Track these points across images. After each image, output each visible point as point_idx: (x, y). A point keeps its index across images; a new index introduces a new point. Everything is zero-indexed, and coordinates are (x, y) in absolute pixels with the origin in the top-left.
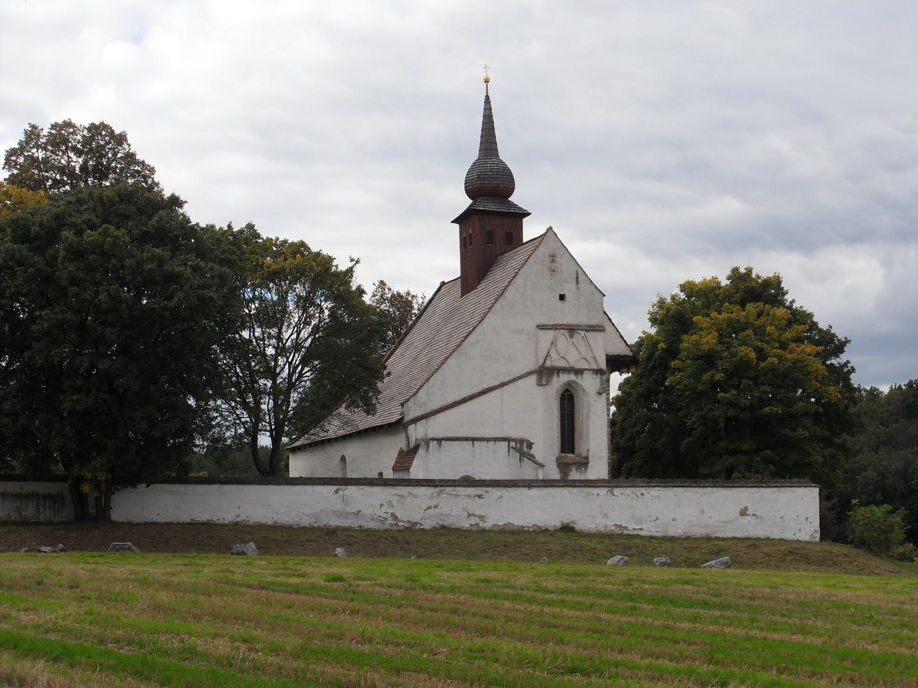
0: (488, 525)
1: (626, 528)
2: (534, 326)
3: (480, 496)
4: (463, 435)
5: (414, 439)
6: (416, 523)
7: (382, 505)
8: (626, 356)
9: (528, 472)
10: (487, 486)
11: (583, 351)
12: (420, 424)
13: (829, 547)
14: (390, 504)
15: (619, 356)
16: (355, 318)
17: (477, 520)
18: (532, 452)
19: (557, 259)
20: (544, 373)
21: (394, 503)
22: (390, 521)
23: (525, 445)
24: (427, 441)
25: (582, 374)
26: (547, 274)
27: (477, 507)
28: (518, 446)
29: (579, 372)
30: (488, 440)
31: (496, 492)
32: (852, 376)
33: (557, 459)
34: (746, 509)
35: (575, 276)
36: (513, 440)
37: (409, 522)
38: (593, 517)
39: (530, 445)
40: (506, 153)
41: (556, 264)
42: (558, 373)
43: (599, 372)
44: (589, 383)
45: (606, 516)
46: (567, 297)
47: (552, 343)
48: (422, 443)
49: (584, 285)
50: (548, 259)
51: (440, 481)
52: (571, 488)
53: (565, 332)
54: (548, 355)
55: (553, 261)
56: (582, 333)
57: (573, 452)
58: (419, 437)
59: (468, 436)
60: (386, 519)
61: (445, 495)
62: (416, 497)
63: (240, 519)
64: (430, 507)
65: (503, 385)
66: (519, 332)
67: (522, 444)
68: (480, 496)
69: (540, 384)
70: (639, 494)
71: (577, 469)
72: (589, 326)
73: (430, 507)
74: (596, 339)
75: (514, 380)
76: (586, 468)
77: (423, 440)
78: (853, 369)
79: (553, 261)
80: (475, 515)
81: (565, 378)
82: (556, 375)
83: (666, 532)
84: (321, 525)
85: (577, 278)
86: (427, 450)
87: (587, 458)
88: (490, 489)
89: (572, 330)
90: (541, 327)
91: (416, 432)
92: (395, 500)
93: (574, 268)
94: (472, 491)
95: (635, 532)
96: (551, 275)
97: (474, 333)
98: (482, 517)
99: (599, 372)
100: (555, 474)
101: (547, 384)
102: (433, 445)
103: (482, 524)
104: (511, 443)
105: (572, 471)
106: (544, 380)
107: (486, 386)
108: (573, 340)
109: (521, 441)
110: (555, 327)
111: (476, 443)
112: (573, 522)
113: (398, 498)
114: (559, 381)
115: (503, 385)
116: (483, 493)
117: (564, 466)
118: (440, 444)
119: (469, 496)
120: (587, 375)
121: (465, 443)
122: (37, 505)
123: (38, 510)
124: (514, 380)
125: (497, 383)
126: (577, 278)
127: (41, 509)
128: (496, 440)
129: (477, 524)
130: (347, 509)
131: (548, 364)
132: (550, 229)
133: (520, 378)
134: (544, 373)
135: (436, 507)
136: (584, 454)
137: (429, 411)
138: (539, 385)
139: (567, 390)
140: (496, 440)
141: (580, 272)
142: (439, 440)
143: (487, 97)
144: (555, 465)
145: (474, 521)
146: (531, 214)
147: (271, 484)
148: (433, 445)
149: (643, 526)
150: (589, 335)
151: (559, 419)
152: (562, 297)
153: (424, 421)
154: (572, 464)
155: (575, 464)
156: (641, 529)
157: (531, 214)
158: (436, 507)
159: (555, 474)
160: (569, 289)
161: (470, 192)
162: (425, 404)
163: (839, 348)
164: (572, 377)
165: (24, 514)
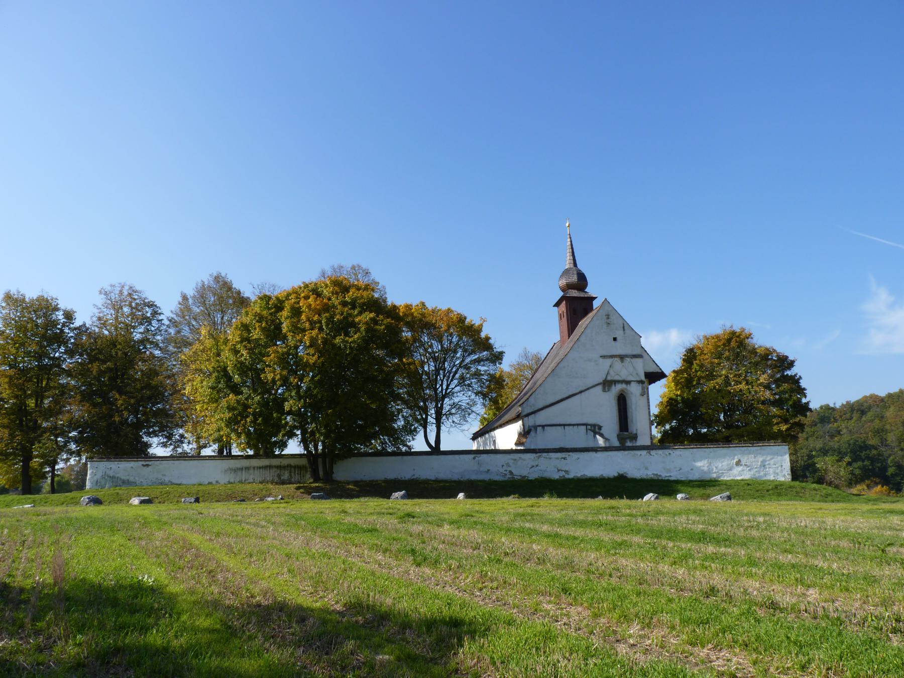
0: (571, 476)
1: (660, 476)
3: (564, 458)
4: (558, 423)
6: (525, 476)
7: (503, 466)
10: (569, 452)
12: (530, 417)
13: (797, 483)
14: (508, 465)
17: (564, 473)
18: (601, 432)
20: (607, 384)
21: (511, 464)
22: (508, 476)
23: (597, 428)
24: (536, 427)
25: (630, 384)
26: (605, 326)
27: (563, 465)
28: (593, 428)
29: (628, 382)
30: (574, 425)
31: (575, 455)
32: (801, 381)
33: (618, 435)
34: (739, 461)
35: (622, 326)
36: (589, 425)
37: (520, 476)
38: (639, 469)
39: (600, 428)
42: (615, 384)
43: (641, 382)
44: (634, 390)
45: (647, 469)
46: (618, 339)
47: (610, 366)
48: (533, 428)
49: (628, 331)
50: (605, 317)
51: (539, 449)
52: (622, 451)
53: (617, 359)
55: (608, 318)
56: (628, 359)
57: (628, 432)
59: (561, 423)
60: (506, 474)
61: (542, 458)
62: (524, 460)
63: (415, 477)
64: (533, 466)
65: (581, 392)
67: (595, 427)
68: (564, 458)
69: (604, 390)
70: (668, 454)
71: (630, 442)
73: (533, 466)
74: (638, 362)
75: (588, 389)
76: (636, 440)
77: (532, 426)
78: (800, 378)
80: (562, 471)
81: (619, 387)
83: (687, 478)
84: (465, 479)
85: (624, 327)
86: (536, 432)
87: (636, 434)
88: (570, 453)
89: (622, 358)
90: (603, 357)
91: (541, 418)
92: (511, 462)
93: (621, 322)
94: (559, 455)
95: (666, 478)
96: (608, 326)
97: (562, 362)
98: (567, 472)
99: (641, 382)
100: (616, 443)
101: (609, 391)
102: (539, 429)
103: (567, 476)
106: (606, 388)
107: (571, 393)
109: (594, 426)
110: (612, 357)
111: (566, 427)
112: (625, 473)
113: (513, 461)
115: (581, 392)
116: (567, 456)
117: (621, 439)
118: (544, 428)
119: (558, 458)
121: (559, 428)
122: (290, 472)
123: (291, 475)
124: (588, 389)
125: (578, 391)
126: (624, 327)
127: (293, 474)
128: (578, 425)
129: (564, 476)
130: (482, 469)
131: (609, 378)
132: (606, 299)
134: (607, 384)
135: (537, 466)
136: (635, 432)
137: (536, 409)
139: (622, 394)
141: (625, 323)
142: (543, 426)
145: (562, 474)
146: (554, 306)
148: (539, 429)
149: (671, 474)
151: (617, 411)
152: (615, 339)
153: (533, 415)
155: (629, 438)
156: (670, 476)
157: (554, 306)
158: (537, 466)
160: (619, 334)
163: (791, 364)
164: (624, 386)
165: (282, 478)
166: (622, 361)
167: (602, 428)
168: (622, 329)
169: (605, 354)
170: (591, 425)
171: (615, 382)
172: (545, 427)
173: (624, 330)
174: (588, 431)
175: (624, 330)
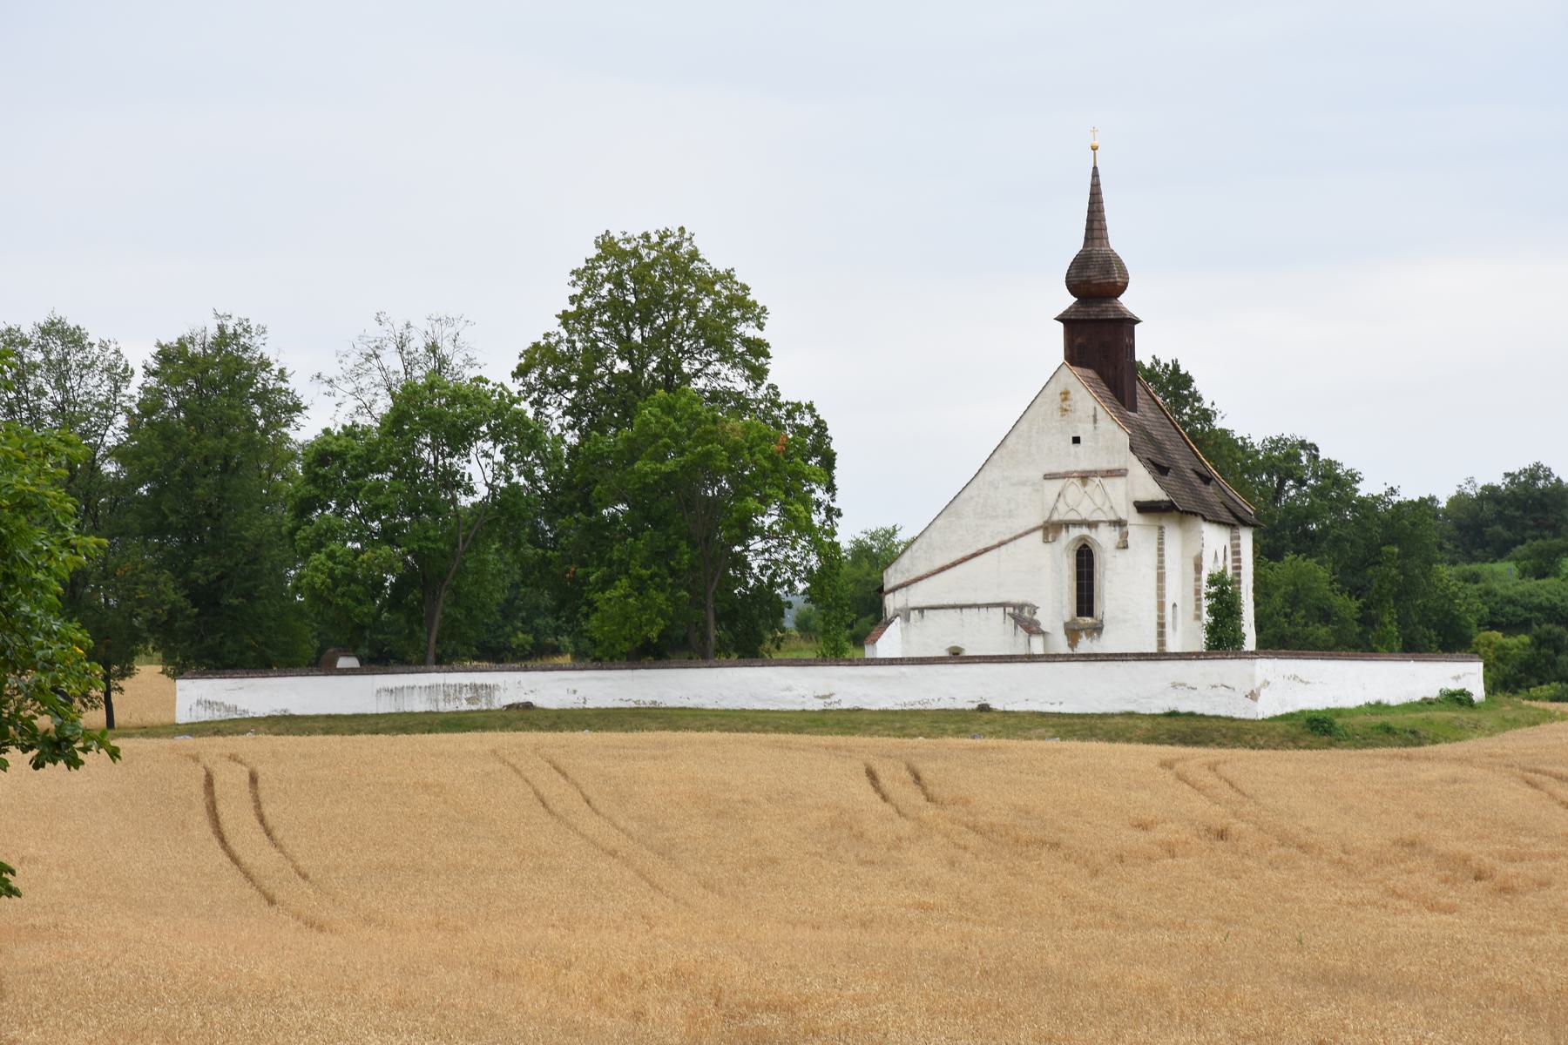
2: (1041, 475)
5: (892, 609)
8: (1163, 501)
9: (1037, 646)
11: (1099, 501)
15: (1153, 502)
16: (450, 511)
19: (1071, 396)
29: (1092, 525)
30: (978, 606)
35: (1092, 413)
39: (1034, 609)
40: (1119, 241)
41: (1068, 403)
43: (1119, 523)
47: (1059, 495)
50: (1059, 398)
54: (1055, 508)
58: (898, 607)
66: (1024, 483)
69: (1046, 541)
71: (1087, 635)
72: (1108, 471)
79: (1065, 399)
81: (1076, 532)
82: (1064, 530)
85: (1095, 416)
89: (1085, 477)
90: (1049, 477)
96: (1062, 416)
100: (1062, 646)
101: (1054, 541)
102: (914, 615)
104: (1007, 609)
105: (1081, 637)
107: (981, 547)
108: (1087, 489)
109: (1021, 607)
111: (964, 610)
114: (1068, 537)
117: (1073, 633)
120: (1103, 529)
124: (1015, 538)
125: (995, 542)
126: (1095, 416)
128: (988, 606)
131: (1056, 518)
133: (1021, 536)
134: (1051, 529)
137: (912, 577)
138: (1045, 542)
139: (1085, 546)
140: (988, 606)
142: (921, 610)
143: (1095, 168)
144: (1062, 632)
147: (690, 667)
148: (914, 615)
150: (1107, 482)
152: (1076, 440)
153: (904, 589)
154: (1082, 630)
159: (1062, 646)
161: (1073, 287)
162: (908, 571)
164: (1085, 531)
166: (1084, 484)
167: (1037, 611)
168: (1092, 419)
169: (1054, 469)
170: (1014, 606)
171: (1067, 525)
172: (925, 611)
173: (1095, 421)
174: (1007, 616)
175: (1095, 421)
